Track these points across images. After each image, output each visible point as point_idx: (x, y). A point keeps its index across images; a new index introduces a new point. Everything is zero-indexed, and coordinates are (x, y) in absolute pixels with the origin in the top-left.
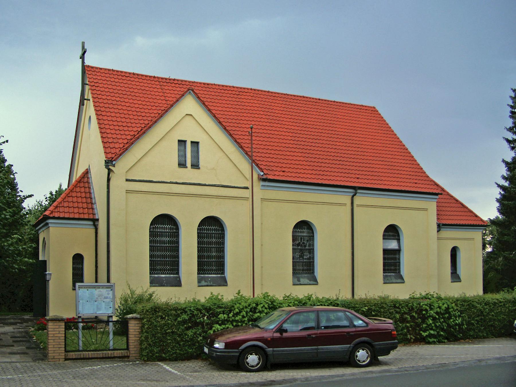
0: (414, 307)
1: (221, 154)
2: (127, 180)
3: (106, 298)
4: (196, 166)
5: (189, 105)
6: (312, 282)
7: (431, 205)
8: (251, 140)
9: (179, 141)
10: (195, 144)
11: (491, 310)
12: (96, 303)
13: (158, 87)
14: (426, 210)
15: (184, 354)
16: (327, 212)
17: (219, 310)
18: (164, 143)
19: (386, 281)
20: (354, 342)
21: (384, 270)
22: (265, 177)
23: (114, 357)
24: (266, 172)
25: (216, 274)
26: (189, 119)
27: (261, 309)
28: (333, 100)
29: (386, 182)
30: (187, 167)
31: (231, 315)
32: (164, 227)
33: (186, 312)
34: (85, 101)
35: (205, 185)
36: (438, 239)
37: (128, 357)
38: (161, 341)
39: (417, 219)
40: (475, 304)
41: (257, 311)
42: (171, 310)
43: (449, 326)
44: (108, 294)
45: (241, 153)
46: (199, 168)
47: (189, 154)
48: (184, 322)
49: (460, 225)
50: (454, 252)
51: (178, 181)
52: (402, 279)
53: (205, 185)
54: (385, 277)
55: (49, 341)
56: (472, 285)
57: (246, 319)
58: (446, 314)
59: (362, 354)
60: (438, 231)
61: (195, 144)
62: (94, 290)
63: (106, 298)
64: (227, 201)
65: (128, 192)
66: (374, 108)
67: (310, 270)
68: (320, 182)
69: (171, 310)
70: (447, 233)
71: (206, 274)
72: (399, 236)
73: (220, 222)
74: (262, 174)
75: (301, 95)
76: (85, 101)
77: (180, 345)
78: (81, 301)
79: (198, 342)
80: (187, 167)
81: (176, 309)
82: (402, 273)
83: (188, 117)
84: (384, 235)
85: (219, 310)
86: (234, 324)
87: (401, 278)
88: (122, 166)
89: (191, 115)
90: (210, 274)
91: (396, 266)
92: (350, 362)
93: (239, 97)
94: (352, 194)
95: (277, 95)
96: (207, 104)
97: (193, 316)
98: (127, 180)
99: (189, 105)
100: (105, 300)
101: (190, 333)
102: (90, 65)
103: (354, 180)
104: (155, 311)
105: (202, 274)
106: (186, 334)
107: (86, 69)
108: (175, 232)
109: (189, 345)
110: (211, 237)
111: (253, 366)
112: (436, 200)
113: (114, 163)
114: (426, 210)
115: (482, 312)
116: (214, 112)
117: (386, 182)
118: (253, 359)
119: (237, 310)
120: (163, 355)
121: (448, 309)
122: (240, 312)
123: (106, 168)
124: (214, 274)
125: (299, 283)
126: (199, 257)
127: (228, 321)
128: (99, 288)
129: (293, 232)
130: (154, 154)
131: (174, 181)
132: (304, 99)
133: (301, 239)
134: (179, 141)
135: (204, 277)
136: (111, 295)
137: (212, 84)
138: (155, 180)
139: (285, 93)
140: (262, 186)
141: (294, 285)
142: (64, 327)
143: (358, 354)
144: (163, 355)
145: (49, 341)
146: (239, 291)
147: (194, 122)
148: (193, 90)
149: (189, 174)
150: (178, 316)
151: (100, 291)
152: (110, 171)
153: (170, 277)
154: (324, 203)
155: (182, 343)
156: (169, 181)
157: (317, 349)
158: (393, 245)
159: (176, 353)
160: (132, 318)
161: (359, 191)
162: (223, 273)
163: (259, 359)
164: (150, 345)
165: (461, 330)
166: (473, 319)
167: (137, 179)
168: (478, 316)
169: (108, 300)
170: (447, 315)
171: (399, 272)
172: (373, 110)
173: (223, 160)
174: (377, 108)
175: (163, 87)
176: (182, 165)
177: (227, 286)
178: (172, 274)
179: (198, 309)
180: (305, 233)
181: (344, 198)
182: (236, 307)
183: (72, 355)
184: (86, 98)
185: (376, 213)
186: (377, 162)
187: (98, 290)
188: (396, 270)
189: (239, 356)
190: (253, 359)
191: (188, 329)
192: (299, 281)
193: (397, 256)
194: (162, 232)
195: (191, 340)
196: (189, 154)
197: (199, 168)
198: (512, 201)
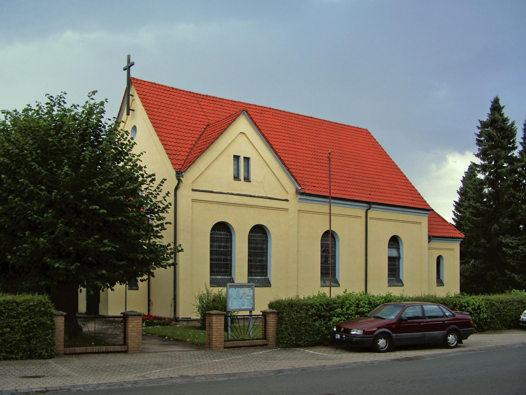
0: (457, 304)
1: (268, 169)
2: (193, 190)
3: (248, 296)
4: (247, 179)
5: (242, 124)
6: (335, 285)
7: (424, 220)
8: (330, 164)
9: (234, 156)
10: (247, 159)
11: (504, 308)
12: (241, 300)
13: (196, 102)
14: (420, 223)
15: (312, 342)
16: (348, 223)
17: (335, 305)
18: (222, 158)
19: (391, 284)
20: (448, 328)
21: (211, 271)
22: (302, 191)
23: (240, 347)
24: (303, 187)
25: (260, 276)
26: (241, 137)
27: (363, 305)
28: (335, 122)
29: (391, 199)
30: (240, 180)
31: (344, 309)
32: (222, 232)
33: (313, 307)
34: (131, 111)
35: (255, 197)
36: (429, 249)
37: (266, 345)
38: (296, 331)
39: (413, 231)
40: (494, 302)
41: (360, 306)
42: (303, 305)
43: (479, 319)
44: (250, 292)
45: (284, 170)
46: (250, 182)
47: (242, 168)
48: (313, 315)
49: (451, 238)
50: (439, 258)
51: (234, 193)
52: (402, 282)
53: (255, 197)
54: (389, 280)
55: (213, 332)
56: (452, 287)
57: (354, 313)
58: (478, 309)
59: (451, 338)
60: (429, 242)
61: (247, 159)
62: (239, 289)
63: (248, 296)
64: (271, 211)
65: (194, 200)
66: (367, 130)
67: (263, 273)
68: (344, 197)
69: (303, 305)
70: (436, 244)
71: (252, 276)
72: (399, 245)
73: (228, 227)
74: (300, 188)
75: (310, 116)
76: (131, 111)
77: (309, 334)
78: (230, 299)
79: (322, 331)
80: (240, 180)
81: (306, 305)
82: (401, 278)
83: (243, 135)
84: (389, 245)
85: (335, 305)
86: (346, 316)
87: (401, 282)
88: (189, 177)
89: (244, 133)
90: (256, 276)
91: (395, 271)
92: (446, 345)
93: (262, 115)
94: (366, 208)
95: (292, 115)
96: (257, 124)
97: (318, 310)
98: (193, 190)
99: (242, 124)
100: (247, 298)
101: (317, 324)
102: (135, 77)
103: (366, 196)
104: (292, 306)
105: (214, 275)
106: (314, 325)
107: (132, 81)
108: (229, 238)
109: (316, 334)
110: (257, 244)
111: (382, 348)
112: (428, 215)
113: (183, 173)
114: (420, 223)
115: (499, 309)
116: (263, 131)
117: (391, 199)
118: (382, 342)
119: (348, 305)
120: (299, 343)
121: (479, 306)
122: (350, 307)
123: (177, 178)
124: (259, 276)
125: (325, 285)
126: (249, 261)
127: (341, 314)
128: (243, 287)
129: (211, 234)
130: (214, 168)
131: (230, 192)
132: (284, 114)
133: (326, 246)
134: (234, 156)
135: (252, 279)
136: (251, 294)
137: (238, 102)
138: (215, 191)
139: (297, 113)
140: (300, 199)
141: (321, 286)
142: (223, 320)
143: (449, 338)
144: (299, 343)
145: (213, 332)
146: (346, 290)
147: (247, 140)
148: (246, 111)
149: (242, 187)
150: (308, 310)
151: (244, 290)
152: (179, 181)
153: (225, 278)
154: (343, 215)
155: (311, 333)
156: (226, 192)
157: (424, 334)
158: (394, 253)
159: (307, 340)
160: (216, 314)
161: (373, 206)
162: (266, 275)
163: (386, 343)
164: (289, 334)
165: (486, 324)
166: (493, 315)
167: (201, 189)
168: (496, 312)
169: (249, 297)
170: (478, 311)
171: (399, 276)
172: (365, 134)
173: (269, 175)
174: (370, 131)
175: (200, 103)
176: (237, 178)
177: (270, 287)
178: (226, 275)
179: (321, 305)
180: (258, 236)
181: (360, 211)
182: (347, 303)
183: (229, 344)
184: (131, 108)
185: (385, 224)
186: (368, 179)
187: (243, 289)
188: (395, 274)
189: (374, 340)
190: (382, 342)
191: (315, 320)
192: (325, 283)
193: (229, 257)
194: (218, 238)
195: (318, 329)
196: (242, 168)
197: (250, 182)
198: (45, 171)
